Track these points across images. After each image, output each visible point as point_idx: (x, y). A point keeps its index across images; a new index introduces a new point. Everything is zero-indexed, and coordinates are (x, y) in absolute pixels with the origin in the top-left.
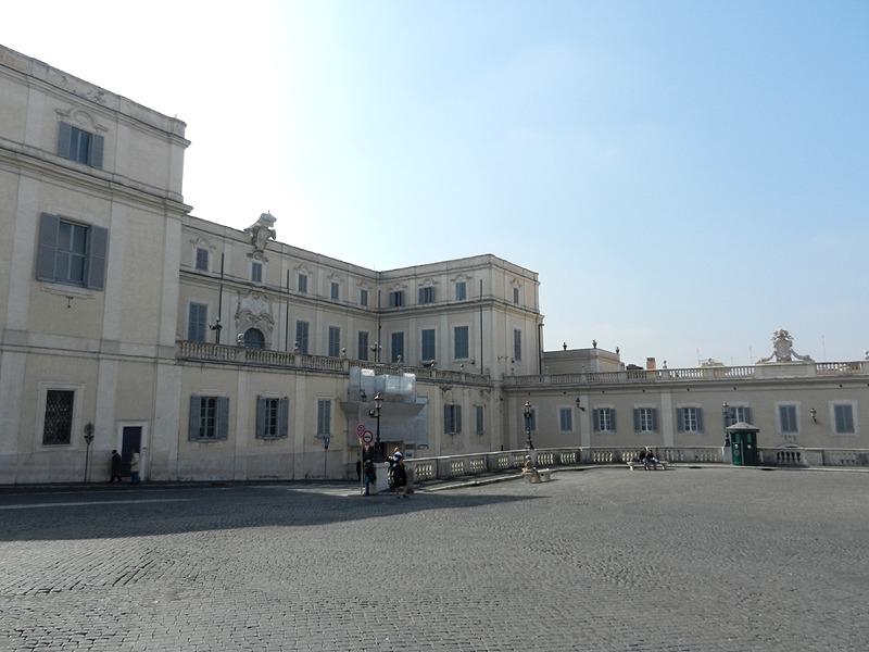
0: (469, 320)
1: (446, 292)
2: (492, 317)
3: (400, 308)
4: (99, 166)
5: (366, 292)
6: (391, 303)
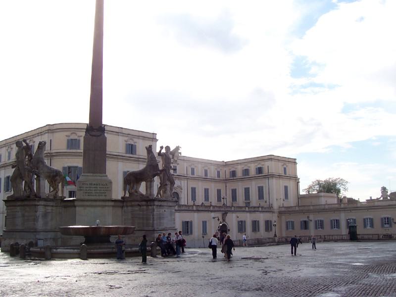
0: (263, 183)
2: (274, 182)
3: (235, 178)
4: (135, 154)
6: (257, 173)
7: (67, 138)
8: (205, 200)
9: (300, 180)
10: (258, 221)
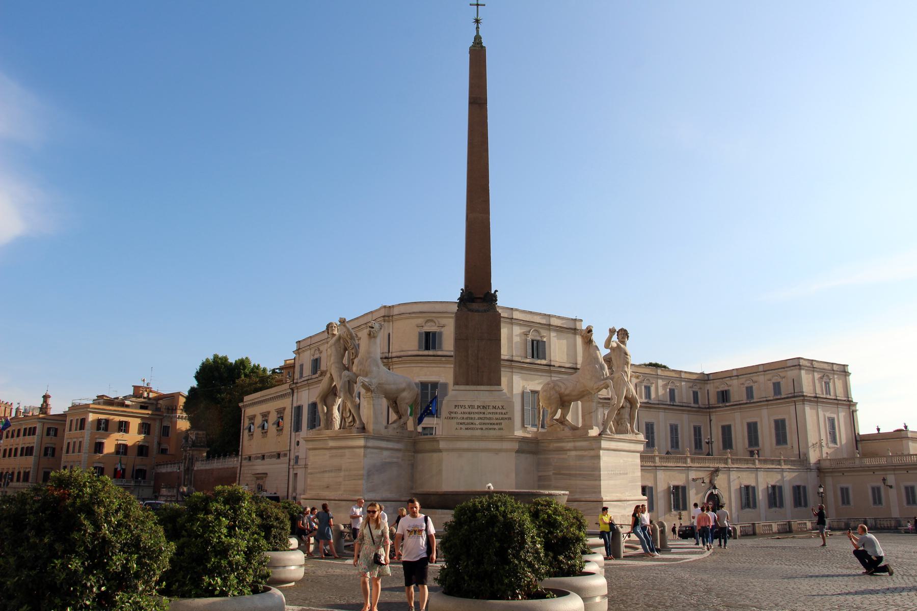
0: (785, 412)
1: (737, 393)
3: (727, 404)
5: (697, 393)
7: (419, 330)
8: (672, 447)
9: (858, 407)
10: (804, 488)
